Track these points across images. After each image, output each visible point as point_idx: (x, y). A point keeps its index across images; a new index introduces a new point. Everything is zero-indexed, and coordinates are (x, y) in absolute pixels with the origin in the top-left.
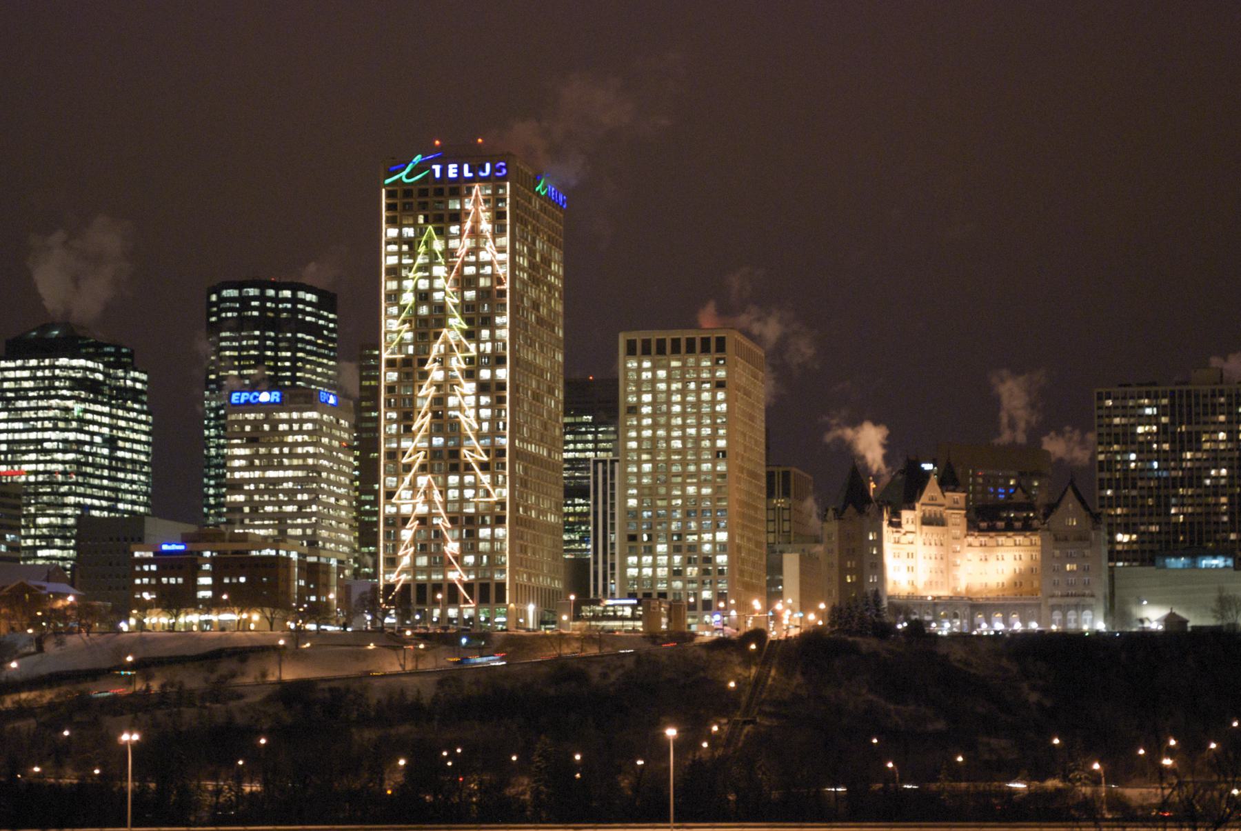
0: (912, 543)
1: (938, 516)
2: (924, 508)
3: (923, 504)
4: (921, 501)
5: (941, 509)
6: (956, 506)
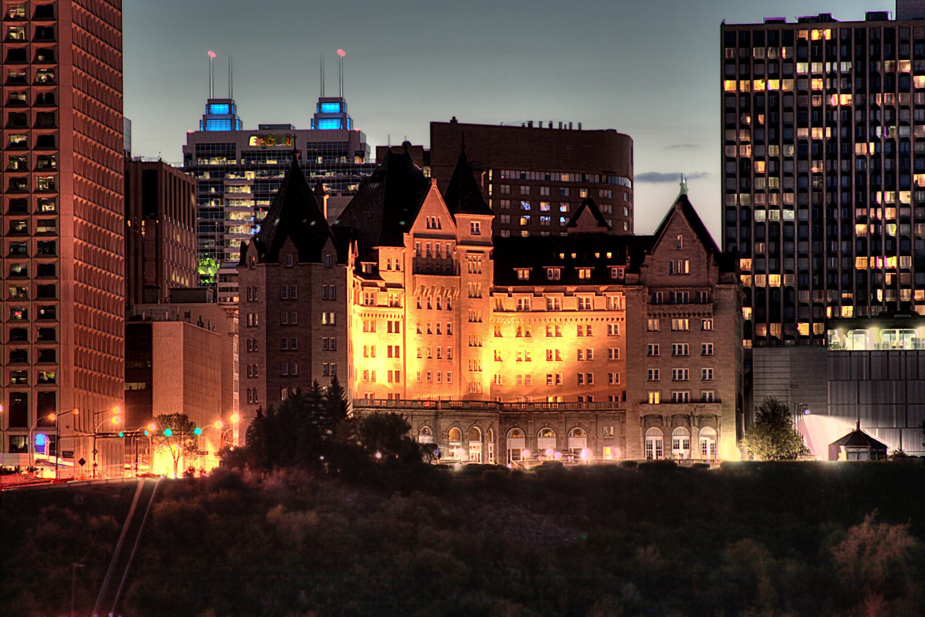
0: (397, 306)
1: (444, 257)
2: (418, 241)
3: (416, 235)
4: (412, 231)
5: (449, 243)
6: (475, 238)
